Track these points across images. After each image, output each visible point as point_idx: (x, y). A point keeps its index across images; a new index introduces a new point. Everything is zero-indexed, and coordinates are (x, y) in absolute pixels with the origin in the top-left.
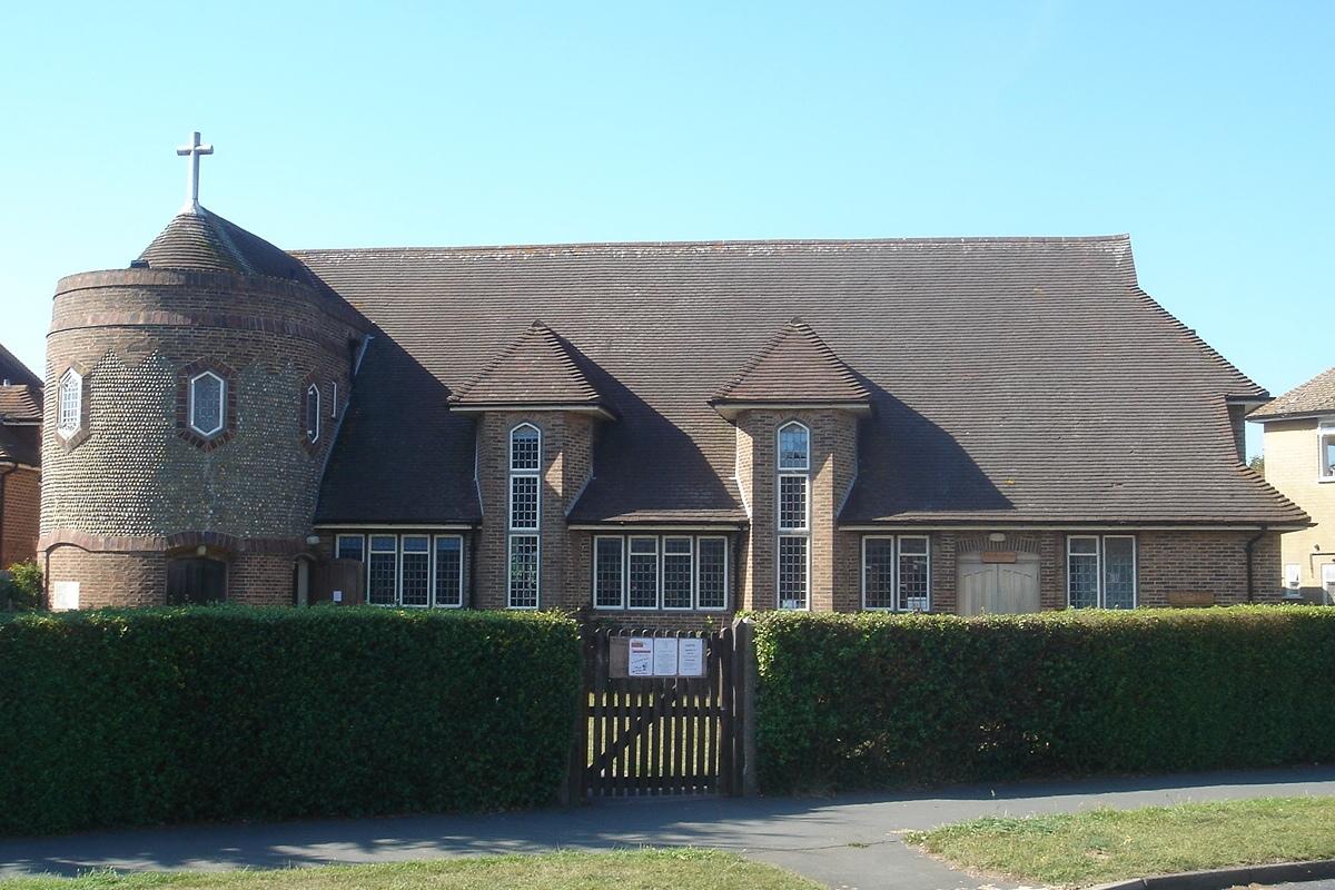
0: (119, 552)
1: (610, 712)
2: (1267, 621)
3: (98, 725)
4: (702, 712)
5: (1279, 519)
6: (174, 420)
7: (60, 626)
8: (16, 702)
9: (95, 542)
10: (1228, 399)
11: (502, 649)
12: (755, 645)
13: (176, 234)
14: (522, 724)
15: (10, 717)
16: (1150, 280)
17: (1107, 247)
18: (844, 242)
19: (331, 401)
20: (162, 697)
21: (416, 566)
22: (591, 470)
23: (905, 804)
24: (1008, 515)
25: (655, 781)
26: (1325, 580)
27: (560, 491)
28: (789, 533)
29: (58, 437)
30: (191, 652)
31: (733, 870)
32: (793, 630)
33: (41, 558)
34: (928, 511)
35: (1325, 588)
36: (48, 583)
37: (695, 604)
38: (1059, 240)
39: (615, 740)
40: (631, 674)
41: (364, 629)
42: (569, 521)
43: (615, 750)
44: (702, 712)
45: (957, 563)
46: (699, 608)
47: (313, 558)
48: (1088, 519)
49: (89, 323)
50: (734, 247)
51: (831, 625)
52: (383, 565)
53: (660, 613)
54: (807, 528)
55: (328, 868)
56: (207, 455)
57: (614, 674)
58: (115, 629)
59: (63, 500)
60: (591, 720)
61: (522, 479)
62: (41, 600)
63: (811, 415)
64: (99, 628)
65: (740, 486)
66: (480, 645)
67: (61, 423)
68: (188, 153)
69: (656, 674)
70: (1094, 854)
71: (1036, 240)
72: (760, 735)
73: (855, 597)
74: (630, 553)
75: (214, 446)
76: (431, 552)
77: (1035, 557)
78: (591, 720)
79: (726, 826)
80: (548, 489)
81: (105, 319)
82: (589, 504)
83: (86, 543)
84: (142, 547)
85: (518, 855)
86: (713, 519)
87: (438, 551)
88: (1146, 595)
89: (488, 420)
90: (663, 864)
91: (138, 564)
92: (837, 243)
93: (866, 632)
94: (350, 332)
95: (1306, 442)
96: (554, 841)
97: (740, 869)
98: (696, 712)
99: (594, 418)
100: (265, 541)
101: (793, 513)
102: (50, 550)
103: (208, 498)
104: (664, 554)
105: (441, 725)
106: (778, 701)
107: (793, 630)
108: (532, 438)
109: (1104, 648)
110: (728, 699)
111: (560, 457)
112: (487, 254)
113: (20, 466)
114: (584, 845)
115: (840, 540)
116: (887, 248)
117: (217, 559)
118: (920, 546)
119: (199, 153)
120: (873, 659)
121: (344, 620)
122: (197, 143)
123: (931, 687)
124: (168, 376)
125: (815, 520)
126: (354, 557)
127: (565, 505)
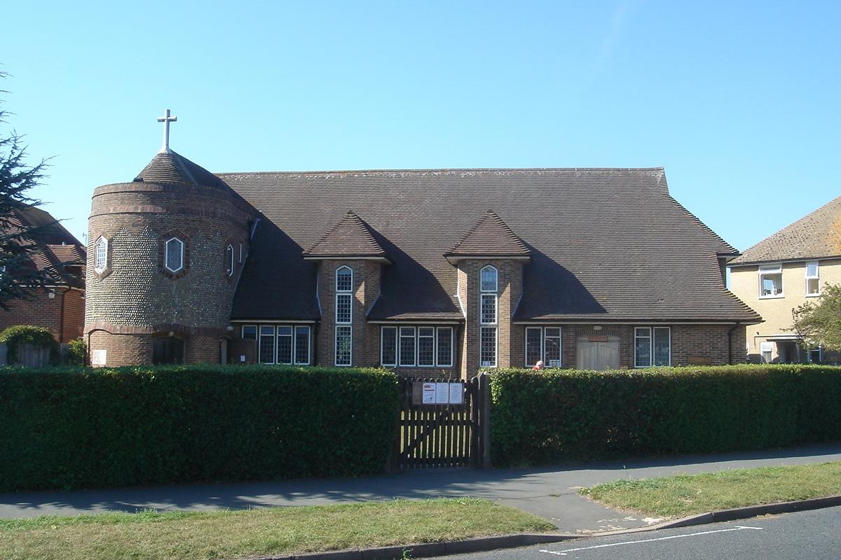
0: (128, 334)
1: (412, 423)
2: (756, 373)
3: (140, 429)
4: (462, 423)
5: (745, 318)
6: (157, 263)
7: (118, 375)
8: (96, 416)
9: (115, 328)
10: (718, 254)
11: (356, 389)
12: (490, 386)
13: (157, 163)
14: (366, 430)
15: (93, 424)
16: (677, 191)
17: (648, 173)
18: (512, 170)
19: (239, 253)
20: (173, 414)
21: (285, 342)
22: (380, 291)
23: (572, 472)
24: (604, 316)
25: (437, 460)
26: (762, 350)
27: (363, 302)
28: (486, 325)
29: (95, 273)
30: (189, 390)
31: (492, 511)
32: (511, 378)
33: (85, 337)
34: (561, 314)
35: (762, 354)
36: (89, 350)
37: (436, 364)
38: (627, 170)
39: (415, 438)
40: (424, 402)
41: (282, 378)
42: (368, 319)
43: (415, 444)
44: (462, 423)
45: (576, 342)
46: (437, 365)
47: (229, 338)
48: (646, 318)
49: (112, 212)
50: (454, 172)
51: (531, 376)
52: (267, 341)
53: (417, 368)
54: (496, 323)
55: (272, 509)
56: (174, 283)
57: (415, 403)
58: (148, 377)
59: (97, 306)
60: (402, 427)
61: (342, 296)
62: (87, 360)
63: (499, 262)
64: (139, 377)
65: (460, 300)
66: (344, 387)
67: (96, 266)
68: (164, 121)
69: (437, 402)
70: (683, 500)
71: (614, 170)
72: (493, 435)
73: (521, 360)
74: (400, 336)
75: (178, 277)
76: (293, 335)
77: (618, 338)
78: (402, 427)
79: (480, 485)
80: (356, 301)
81: (119, 209)
82: (379, 309)
83: (110, 329)
84: (139, 331)
85: (374, 502)
86: (445, 318)
87: (297, 335)
88: (676, 359)
89: (324, 264)
90: (455, 507)
91: (138, 341)
92: (509, 170)
93: (550, 379)
94: (249, 217)
95: (753, 277)
96: (390, 494)
97: (497, 510)
98: (458, 423)
99: (381, 263)
100: (205, 329)
101: (489, 315)
102: (90, 333)
103: (175, 306)
104: (419, 336)
105: (323, 430)
106: (503, 417)
107: (511, 378)
108: (348, 274)
109: (674, 388)
110: (475, 416)
111: (363, 284)
112: (321, 176)
113: (72, 288)
114: (406, 496)
115: (514, 329)
116: (536, 174)
117: (179, 338)
118: (555, 332)
119: (169, 121)
120: (553, 394)
121: (271, 373)
122: (169, 116)
123: (583, 409)
124: (153, 240)
125: (501, 319)
126: (251, 338)
127: (366, 310)
